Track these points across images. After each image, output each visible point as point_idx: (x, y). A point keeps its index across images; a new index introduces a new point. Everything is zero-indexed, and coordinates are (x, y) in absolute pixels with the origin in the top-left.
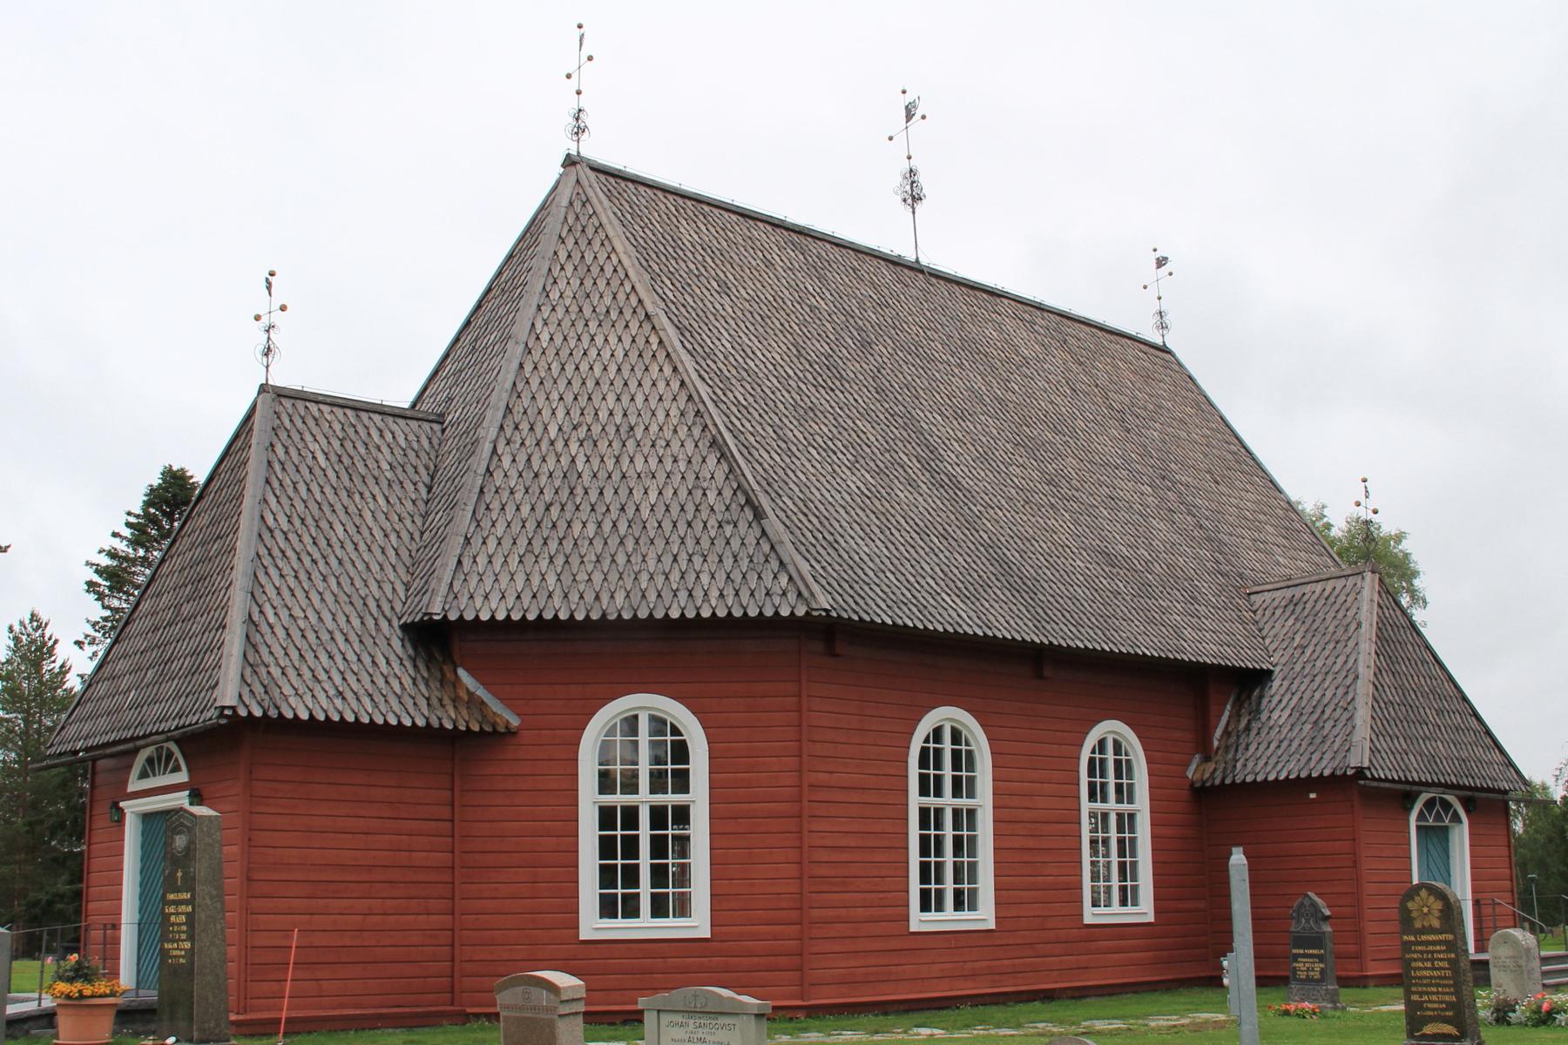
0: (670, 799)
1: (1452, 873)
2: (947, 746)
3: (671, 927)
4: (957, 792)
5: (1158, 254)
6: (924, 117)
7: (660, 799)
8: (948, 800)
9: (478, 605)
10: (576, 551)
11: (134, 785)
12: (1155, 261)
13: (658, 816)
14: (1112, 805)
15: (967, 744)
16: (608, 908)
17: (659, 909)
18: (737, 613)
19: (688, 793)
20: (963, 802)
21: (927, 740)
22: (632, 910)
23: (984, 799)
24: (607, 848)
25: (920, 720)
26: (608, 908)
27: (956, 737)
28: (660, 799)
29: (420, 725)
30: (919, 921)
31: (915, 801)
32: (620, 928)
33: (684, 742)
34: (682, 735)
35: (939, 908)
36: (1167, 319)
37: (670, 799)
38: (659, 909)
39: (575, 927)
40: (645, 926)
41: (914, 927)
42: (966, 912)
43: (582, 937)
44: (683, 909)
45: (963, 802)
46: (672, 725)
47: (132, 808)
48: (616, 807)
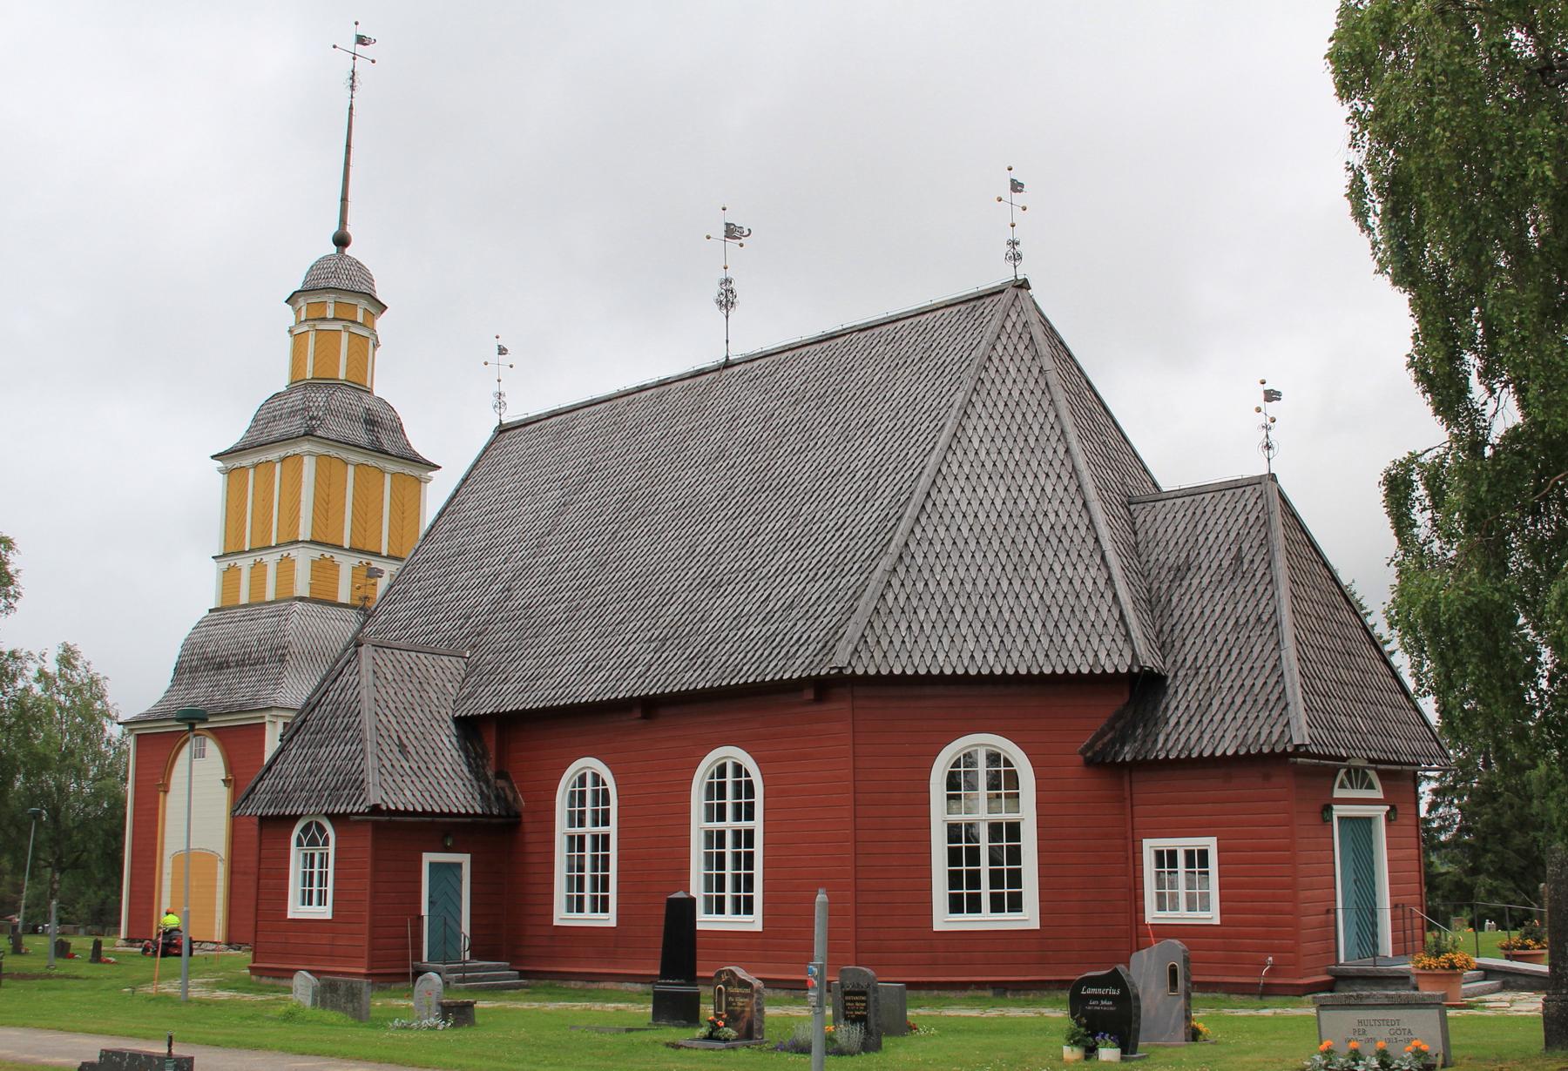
1: (1376, 869)
2: (729, 779)
3: (1007, 921)
4: (737, 818)
5: (1267, 387)
6: (741, 245)
7: (996, 817)
8: (589, 829)
11: (1338, 793)
12: (723, 228)
13: (995, 829)
16: (955, 906)
17: (997, 906)
18: (1072, 671)
20: (577, 830)
21: (957, 764)
22: (975, 906)
24: (954, 856)
26: (955, 906)
27: (994, 758)
30: (943, 919)
31: (757, 825)
32: (966, 922)
33: (751, 781)
35: (310, 903)
36: (495, 400)
38: (997, 906)
40: (986, 920)
41: (938, 926)
42: (714, 915)
44: (1016, 904)
45: (577, 830)
46: (746, 770)
47: (1339, 811)
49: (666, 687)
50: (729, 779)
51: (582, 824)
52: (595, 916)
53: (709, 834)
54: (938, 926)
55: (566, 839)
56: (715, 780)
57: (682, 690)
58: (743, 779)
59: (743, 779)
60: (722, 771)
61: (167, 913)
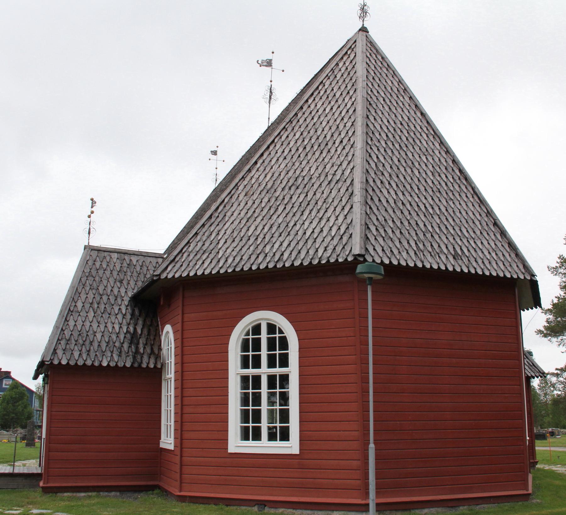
0: (278, 371)
2: (264, 336)
4: (271, 364)
7: (273, 371)
9: (77, 358)
10: (106, 328)
14: (264, 371)
16: (245, 437)
17: (272, 437)
19: (260, 368)
20: (251, 371)
22: (257, 436)
25: (231, 335)
26: (245, 437)
28: (273, 371)
29: (487, 274)
33: (285, 337)
34: (284, 334)
37: (278, 371)
39: (227, 449)
41: (232, 449)
42: (278, 442)
43: (229, 451)
44: (285, 436)
45: (251, 371)
46: (279, 328)
48: (276, 375)
49: (175, 273)
50: (264, 336)
51: (257, 364)
52: (273, 443)
53: (245, 379)
54: (232, 449)
55: (239, 379)
56: (251, 337)
57: (213, 273)
58: (277, 335)
59: (277, 335)
60: (257, 329)
61: (171, 443)
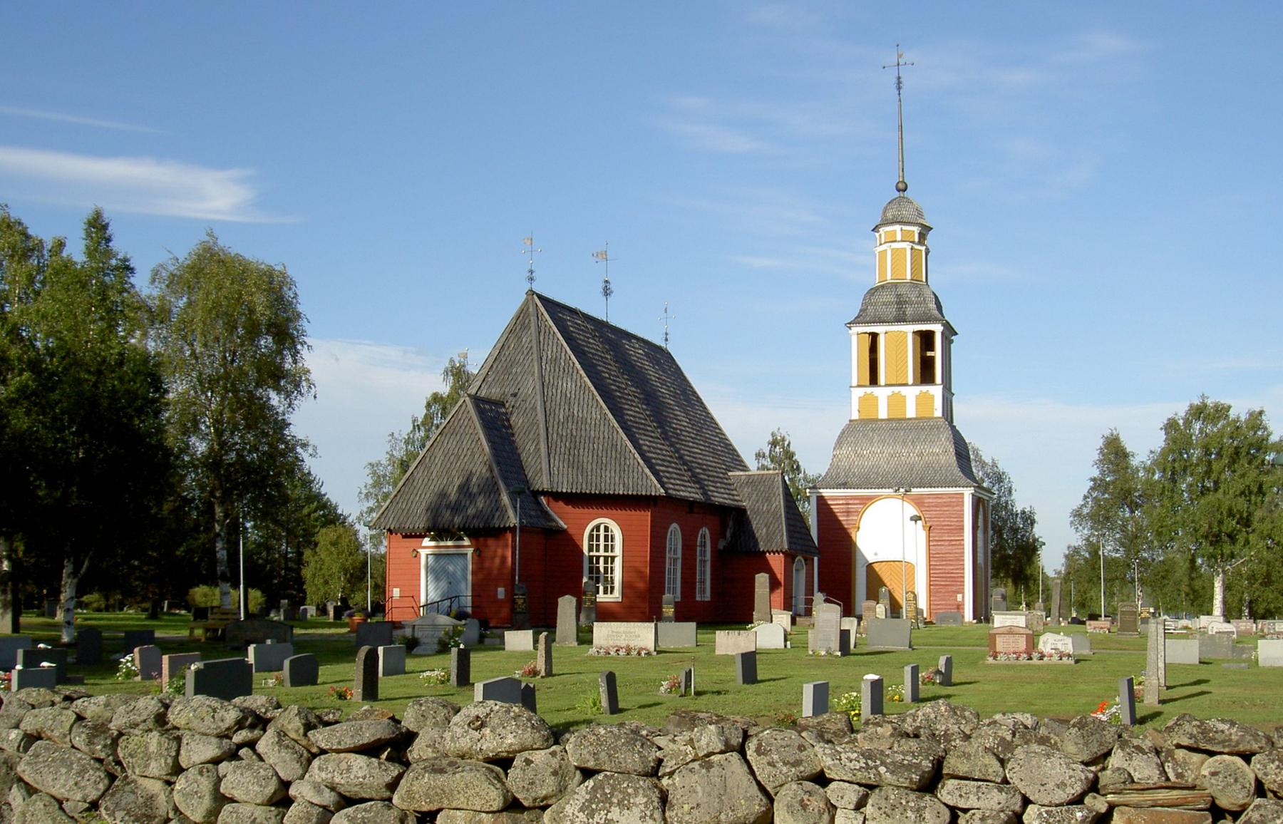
15: (612, 531)
21: (592, 530)
23: (618, 551)
27: (606, 529)
52: (606, 596)
